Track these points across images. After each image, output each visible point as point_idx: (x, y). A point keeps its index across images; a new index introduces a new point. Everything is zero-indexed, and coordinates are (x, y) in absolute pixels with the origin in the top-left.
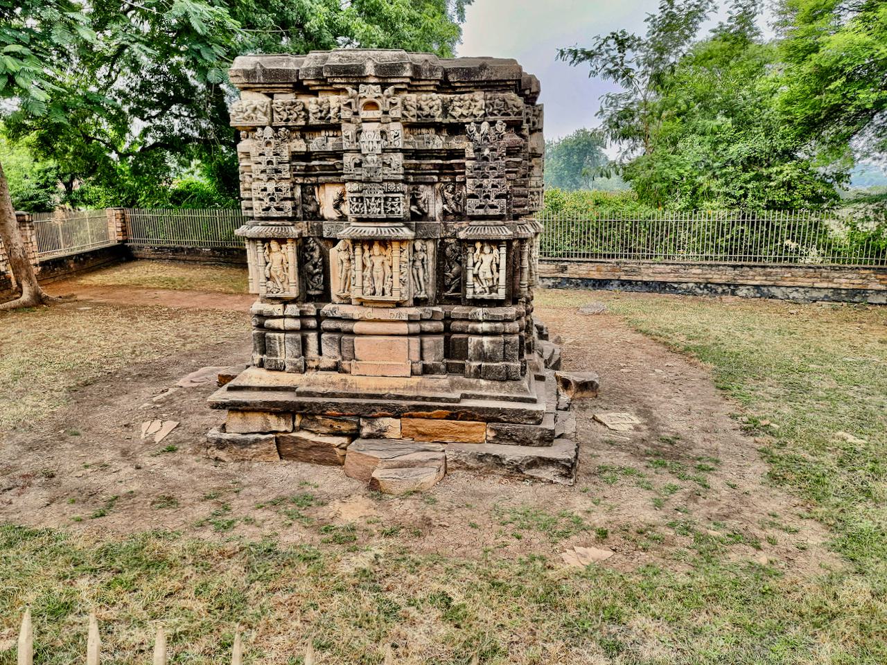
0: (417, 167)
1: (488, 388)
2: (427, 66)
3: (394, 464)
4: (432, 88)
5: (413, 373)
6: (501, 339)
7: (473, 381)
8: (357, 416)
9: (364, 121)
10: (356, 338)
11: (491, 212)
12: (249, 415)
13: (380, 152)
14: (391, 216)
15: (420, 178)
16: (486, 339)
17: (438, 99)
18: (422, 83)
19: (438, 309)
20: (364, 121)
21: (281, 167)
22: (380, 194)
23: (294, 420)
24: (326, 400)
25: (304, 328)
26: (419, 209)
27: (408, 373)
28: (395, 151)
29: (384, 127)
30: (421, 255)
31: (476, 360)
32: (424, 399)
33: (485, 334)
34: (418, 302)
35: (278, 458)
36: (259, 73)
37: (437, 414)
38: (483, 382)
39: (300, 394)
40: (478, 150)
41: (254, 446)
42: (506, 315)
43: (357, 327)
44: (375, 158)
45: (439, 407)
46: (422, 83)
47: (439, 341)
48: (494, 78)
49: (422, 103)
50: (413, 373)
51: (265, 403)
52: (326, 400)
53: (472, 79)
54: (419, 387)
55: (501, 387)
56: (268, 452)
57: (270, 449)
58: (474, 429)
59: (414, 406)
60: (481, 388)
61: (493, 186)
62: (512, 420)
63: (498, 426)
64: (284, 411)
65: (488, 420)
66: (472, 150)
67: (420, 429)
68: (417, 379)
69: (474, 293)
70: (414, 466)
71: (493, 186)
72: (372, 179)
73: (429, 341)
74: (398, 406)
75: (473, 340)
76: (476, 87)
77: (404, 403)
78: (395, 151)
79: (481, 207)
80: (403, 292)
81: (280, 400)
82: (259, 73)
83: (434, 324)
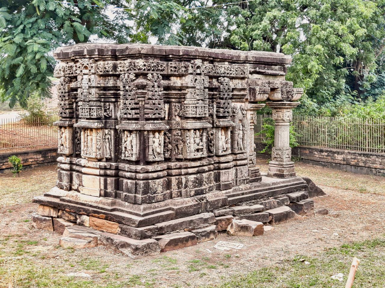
0: (104, 94)
1: (128, 207)
2: (106, 50)
3: (74, 235)
4: (110, 59)
5: (100, 195)
6: (134, 181)
7: (123, 202)
8: (77, 212)
9: (84, 74)
10: (83, 176)
11: (129, 116)
12: (45, 207)
13: (87, 88)
14: (92, 117)
15: (107, 100)
16: (129, 181)
17: (111, 63)
18: (106, 57)
19: (113, 164)
20: (84, 74)
21: (65, 94)
22: (87, 107)
23: (58, 212)
24: (66, 203)
25: (71, 170)
26: (108, 114)
27: (98, 195)
28: (93, 87)
29: (90, 77)
30: (107, 136)
31: (126, 192)
32: (99, 208)
33: (129, 178)
34: (108, 160)
35: (52, 230)
36: (61, 54)
37: (102, 216)
38: (127, 204)
39: (61, 200)
40: (124, 87)
41: (44, 222)
42: (136, 169)
43: (84, 170)
44: (86, 90)
45: (102, 213)
46: (106, 57)
47: (112, 180)
48: (130, 53)
49: (106, 66)
50: (100, 195)
51: (48, 202)
52: (66, 203)
53: (124, 54)
54: (101, 202)
55: (132, 207)
56: (49, 226)
57: (50, 225)
58: (113, 226)
59: (94, 211)
60: (125, 207)
61: (130, 104)
62: (127, 223)
63: (121, 225)
64: (56, 207)
65: (120, 223)
66: (122, 87)
67: (95, 223)
68: (101, 198)
69: (125, 156)
70: (81, 238)
71: (130, 104)
72: (85, 100)
73: (109, 180)
74: (88, 210)
75: (125, 181)
76: (128, 57)
77: (91, 209)
78: (93, 87)
79: (125, 114)
80: (98, 153)
81: (55, 201)
82: (61, 54)
83: (111, 171)
